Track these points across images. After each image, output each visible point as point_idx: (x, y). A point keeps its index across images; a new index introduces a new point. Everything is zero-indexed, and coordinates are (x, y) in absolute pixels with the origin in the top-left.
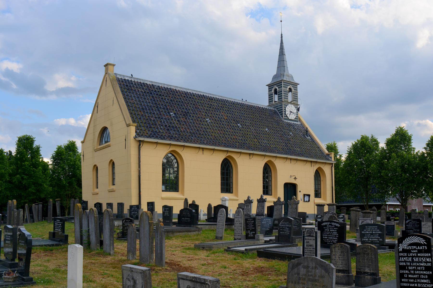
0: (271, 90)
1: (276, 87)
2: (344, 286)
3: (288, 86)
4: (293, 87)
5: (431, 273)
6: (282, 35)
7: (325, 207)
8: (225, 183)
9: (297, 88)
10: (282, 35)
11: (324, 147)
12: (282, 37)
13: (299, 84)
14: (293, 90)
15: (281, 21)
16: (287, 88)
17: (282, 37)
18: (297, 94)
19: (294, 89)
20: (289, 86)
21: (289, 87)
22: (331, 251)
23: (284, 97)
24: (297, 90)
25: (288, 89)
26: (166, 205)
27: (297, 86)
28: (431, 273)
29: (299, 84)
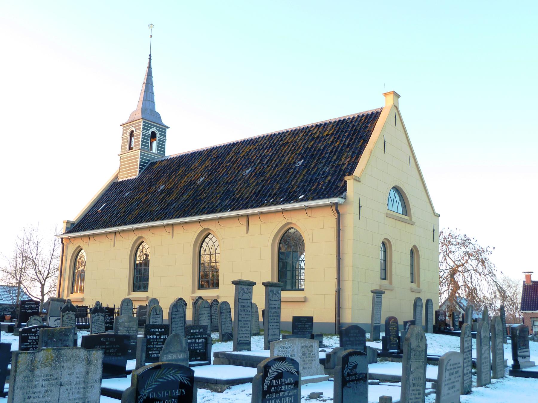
0: (126, 133)
1: (133, 128)
2: (392, 361)
3: (151, 128)
4: (159, 130)
5: (119, 346)
6: (150, 56)
7: (254, 287)
8: (138, 277)
9: (165, 133)
10: (150, 56)
11: (440, 231)
12: (150, 59)
13: (169, 128)
14: (158, 135)
15: (151, 36)
16: (149, 130)
17: (150, 59)
18: (165, 142)
19: (160, 134)
20: (153, 129)
21: (151, 130)
22: (80, 348)
23: (142, 144)
24: (165, 136)
25: (150, 133)
26: (395, 316)
27: (166, 130)
28: (119, 346)
29: (169, 128)
